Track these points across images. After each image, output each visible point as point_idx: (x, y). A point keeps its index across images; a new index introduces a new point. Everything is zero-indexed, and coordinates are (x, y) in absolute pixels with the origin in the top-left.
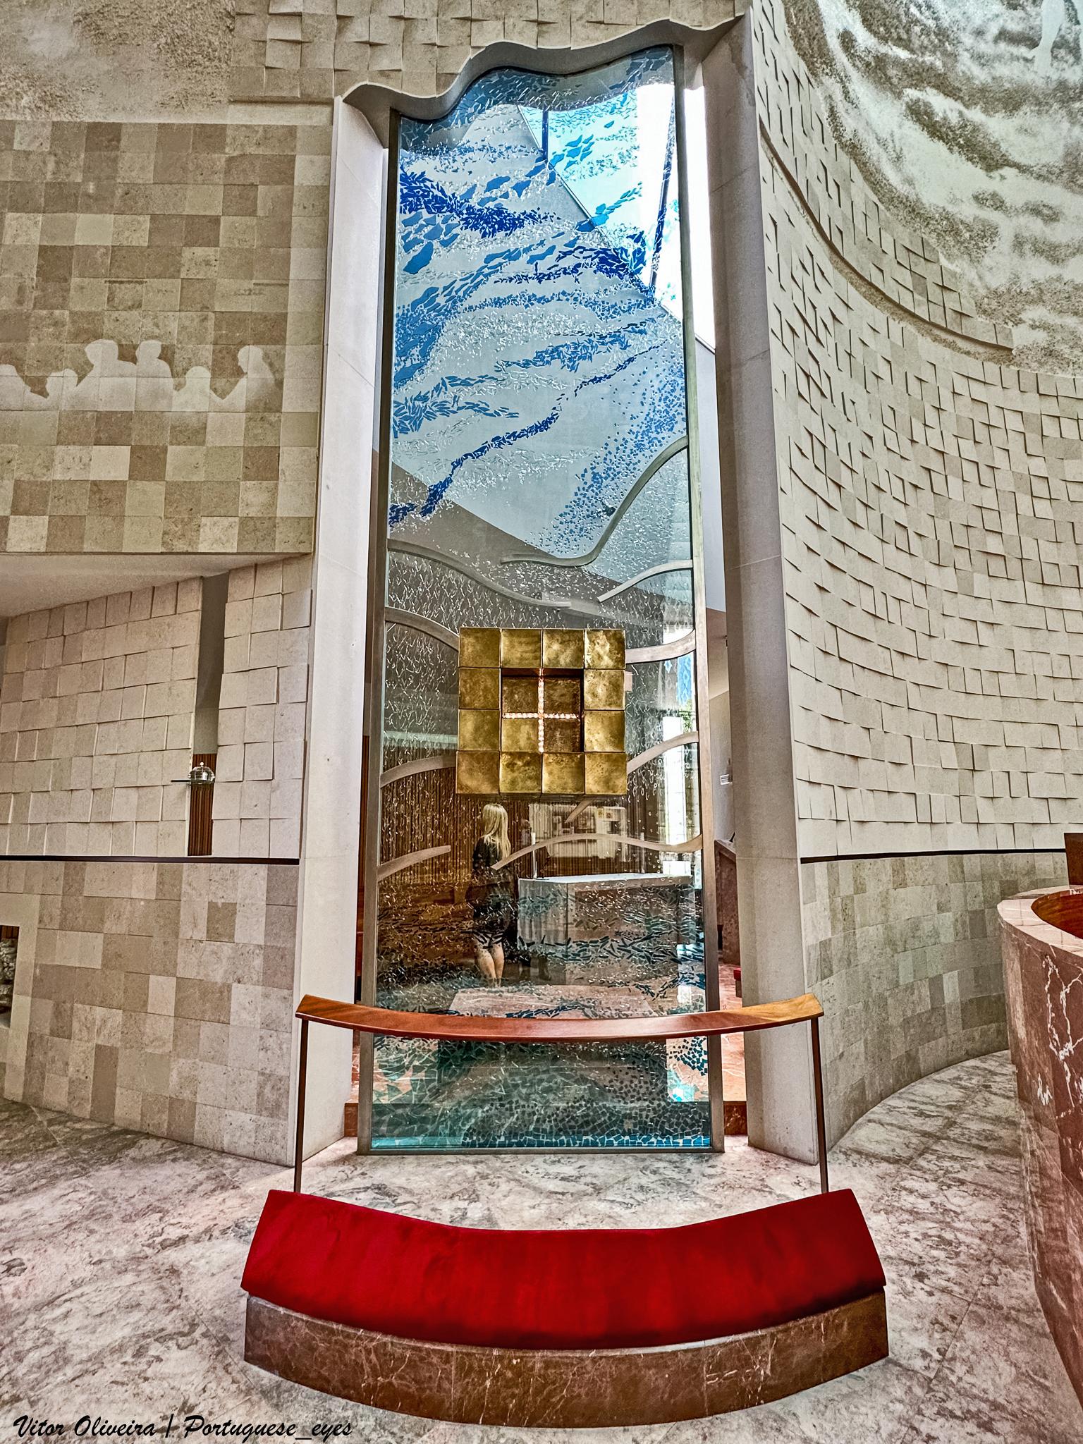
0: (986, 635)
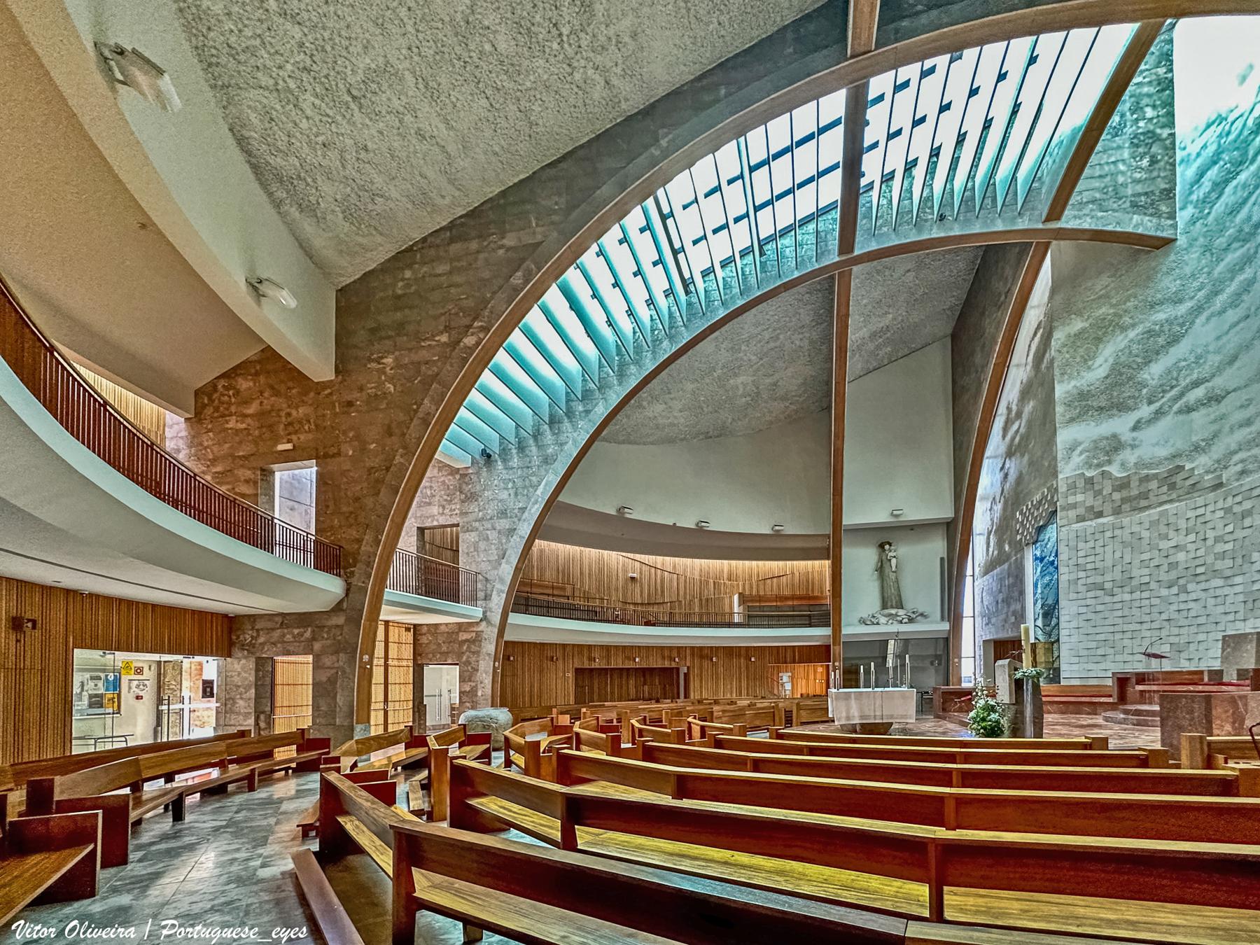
0: (1191, 605)
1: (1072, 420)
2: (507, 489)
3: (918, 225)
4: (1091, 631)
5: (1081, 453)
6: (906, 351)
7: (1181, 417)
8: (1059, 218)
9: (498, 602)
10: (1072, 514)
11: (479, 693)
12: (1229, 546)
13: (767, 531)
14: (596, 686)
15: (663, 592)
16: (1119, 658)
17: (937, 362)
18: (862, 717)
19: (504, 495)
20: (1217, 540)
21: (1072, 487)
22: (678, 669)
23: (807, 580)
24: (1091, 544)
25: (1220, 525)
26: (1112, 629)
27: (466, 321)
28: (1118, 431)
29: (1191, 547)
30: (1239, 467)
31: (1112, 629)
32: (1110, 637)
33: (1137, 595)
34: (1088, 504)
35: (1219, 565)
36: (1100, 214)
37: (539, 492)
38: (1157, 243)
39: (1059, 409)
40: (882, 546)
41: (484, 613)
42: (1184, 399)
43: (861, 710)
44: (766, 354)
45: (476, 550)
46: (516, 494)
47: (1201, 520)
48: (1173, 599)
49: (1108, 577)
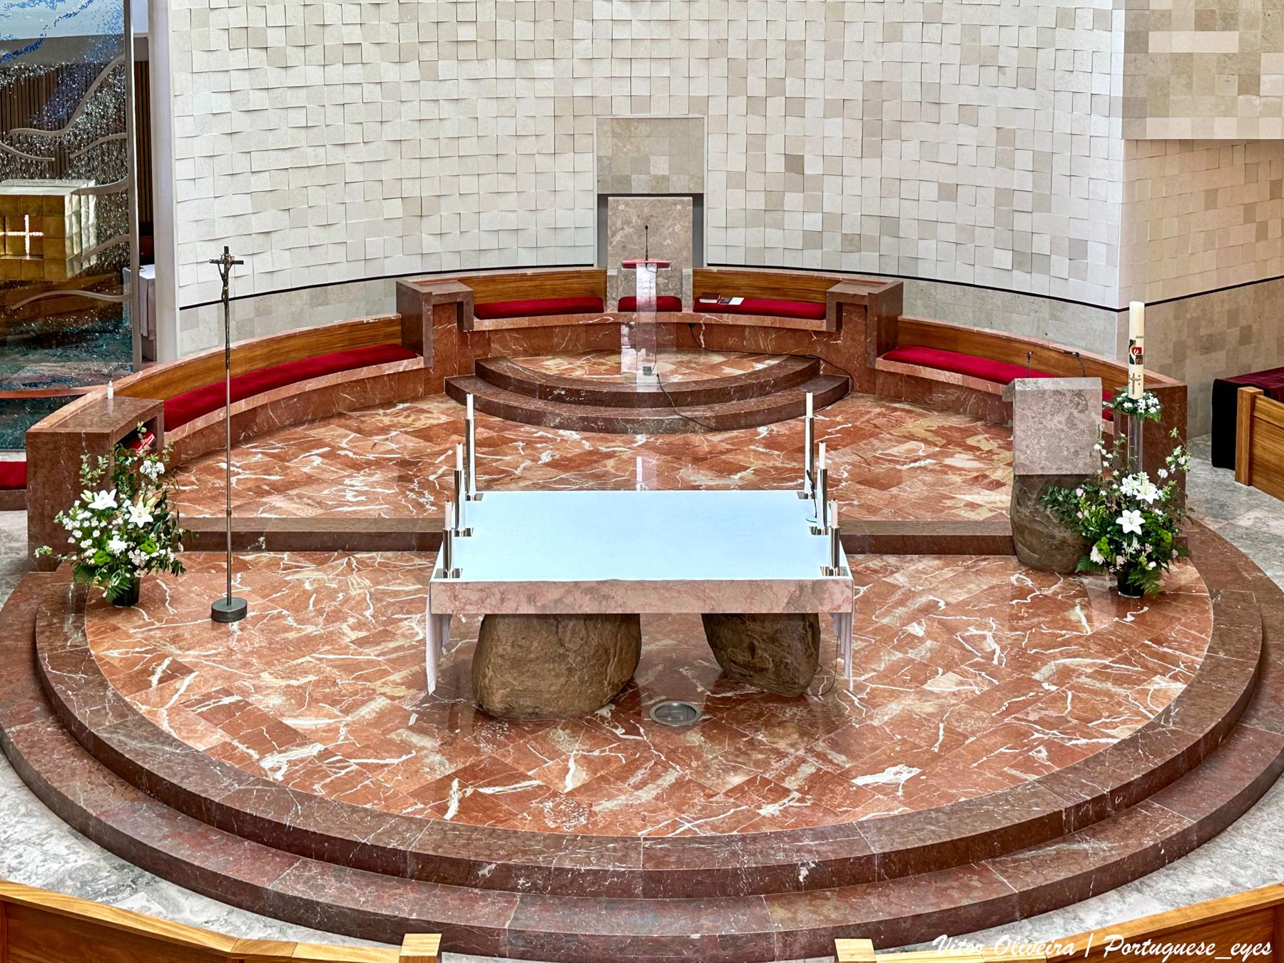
0: (447, 110)
4: (241, 164)
26: (286, 160)
31: (286, 160)
33: (335, 72)
35: (505, 31)
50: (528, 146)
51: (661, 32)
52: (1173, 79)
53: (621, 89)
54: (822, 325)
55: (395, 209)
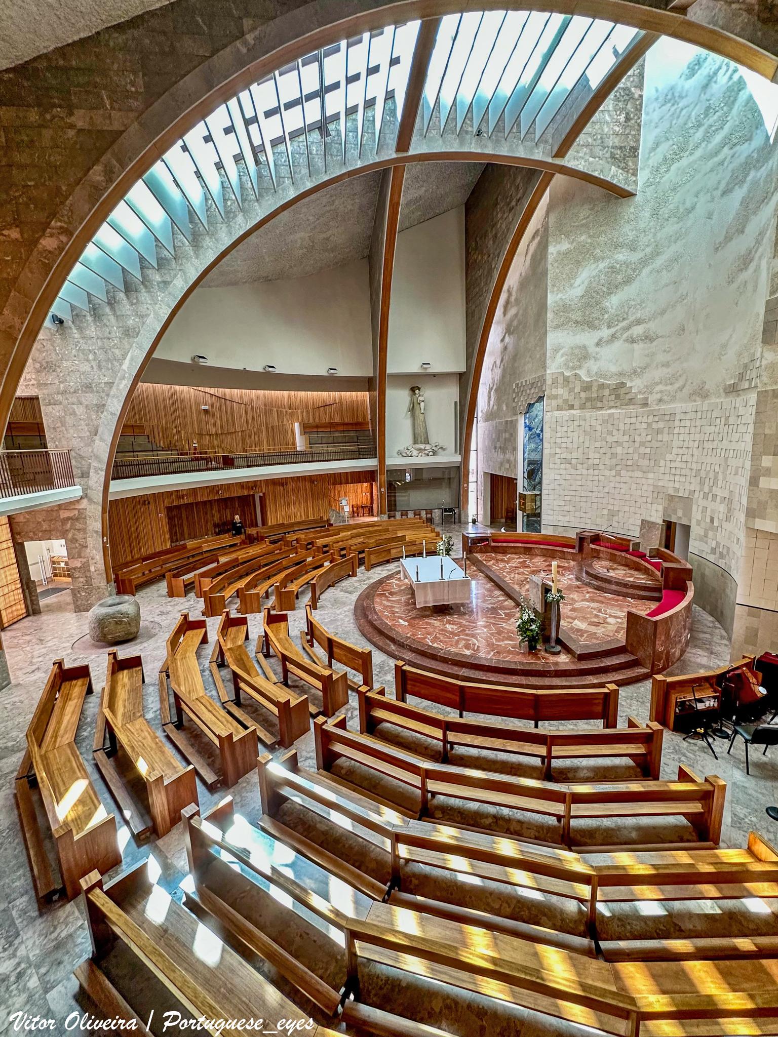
0: (622, 485)
1: (557, 327)
2: (88, 360)
3: (462, 134)
4: (562, 492)
5: (562, 356)
6: (432, 215)
7: (627, 345)
8: (563, 156)
9: (97, 479)
10: (554, 403)
11: (92, 569)
12: (648, 451)
13: (323, 373)
14: (184, 516)
15: (233, 422)
16: (577, 514)
17: (452, 228)
18: (435, 601)
19: (85, 367)
20: (642, 444)
21: (555, 382)
22: (253, 496)
23: (353, 408)
24: (565, 429)
25: (644, 434)
26: (574, 493)
27: (42, 216)
28: (587, 343)
29: (626, 445)
30: (658, 396)
31: (574, 493)
32: (573, 499)
34: (565, 398)
36: (591, 159)
37: (125, 367)
38: (626, 194)
39: (550, 315)
40: (413, 390)
41: (84, 490)
42: (630, 332)
43: (434, 595)
44: (323, 215)
45: (63, 424)
46: (100, 367)
47: (633, 427)
48: (612, 479)
49: (574, 455)
50: (644, 499)
51: (684, 465)
52: (769, 502)
53: (671, 484)
54: (574, 551)
55: (605, 512)
